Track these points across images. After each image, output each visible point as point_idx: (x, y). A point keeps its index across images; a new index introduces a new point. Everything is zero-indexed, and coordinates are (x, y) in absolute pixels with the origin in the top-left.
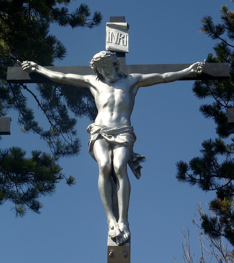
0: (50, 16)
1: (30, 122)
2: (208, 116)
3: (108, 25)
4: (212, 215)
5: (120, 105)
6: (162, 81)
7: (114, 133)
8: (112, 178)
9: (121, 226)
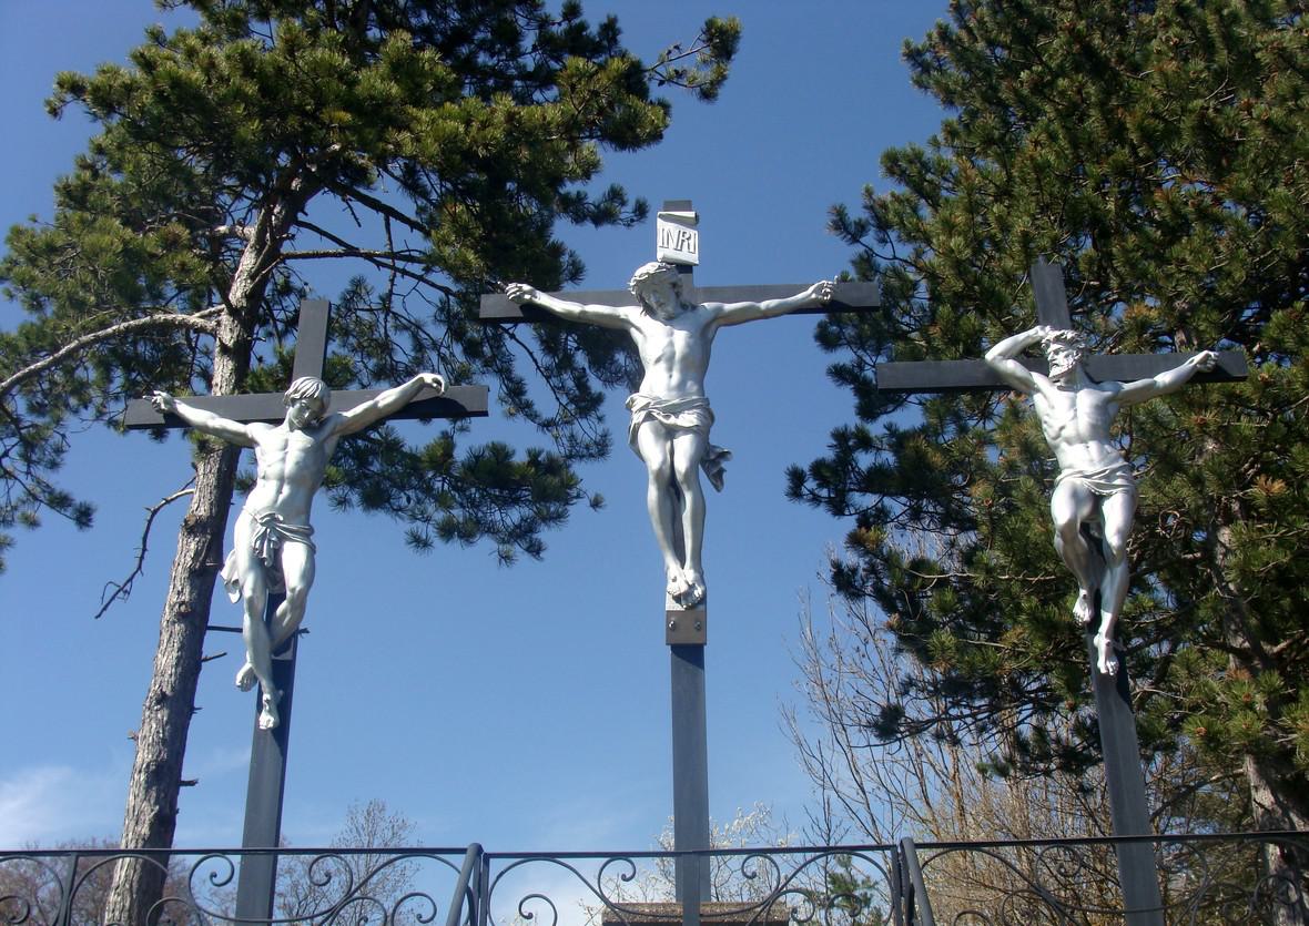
0: (555, 207)
1: (520, 400)
2: (841, 385)
3: (661, 216)
4: (851, 559)
5: (684, 358)
6: (758, 315)
7: (675, 410)
8: (672, 490)
9: (689, 574)
